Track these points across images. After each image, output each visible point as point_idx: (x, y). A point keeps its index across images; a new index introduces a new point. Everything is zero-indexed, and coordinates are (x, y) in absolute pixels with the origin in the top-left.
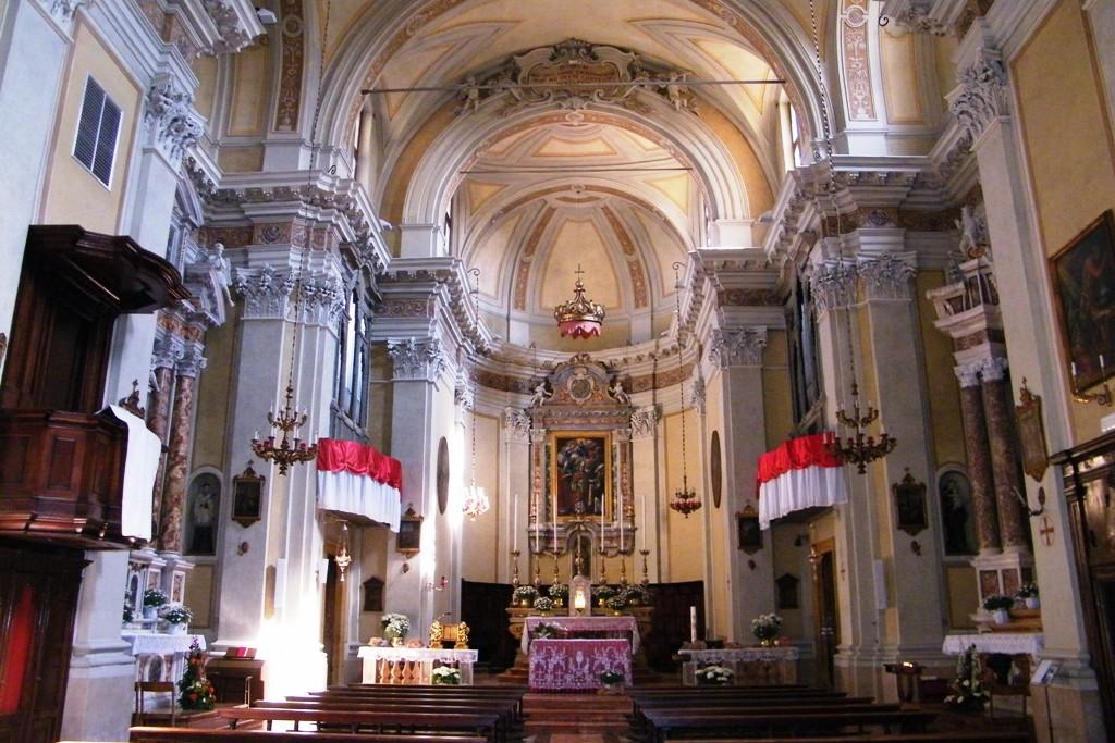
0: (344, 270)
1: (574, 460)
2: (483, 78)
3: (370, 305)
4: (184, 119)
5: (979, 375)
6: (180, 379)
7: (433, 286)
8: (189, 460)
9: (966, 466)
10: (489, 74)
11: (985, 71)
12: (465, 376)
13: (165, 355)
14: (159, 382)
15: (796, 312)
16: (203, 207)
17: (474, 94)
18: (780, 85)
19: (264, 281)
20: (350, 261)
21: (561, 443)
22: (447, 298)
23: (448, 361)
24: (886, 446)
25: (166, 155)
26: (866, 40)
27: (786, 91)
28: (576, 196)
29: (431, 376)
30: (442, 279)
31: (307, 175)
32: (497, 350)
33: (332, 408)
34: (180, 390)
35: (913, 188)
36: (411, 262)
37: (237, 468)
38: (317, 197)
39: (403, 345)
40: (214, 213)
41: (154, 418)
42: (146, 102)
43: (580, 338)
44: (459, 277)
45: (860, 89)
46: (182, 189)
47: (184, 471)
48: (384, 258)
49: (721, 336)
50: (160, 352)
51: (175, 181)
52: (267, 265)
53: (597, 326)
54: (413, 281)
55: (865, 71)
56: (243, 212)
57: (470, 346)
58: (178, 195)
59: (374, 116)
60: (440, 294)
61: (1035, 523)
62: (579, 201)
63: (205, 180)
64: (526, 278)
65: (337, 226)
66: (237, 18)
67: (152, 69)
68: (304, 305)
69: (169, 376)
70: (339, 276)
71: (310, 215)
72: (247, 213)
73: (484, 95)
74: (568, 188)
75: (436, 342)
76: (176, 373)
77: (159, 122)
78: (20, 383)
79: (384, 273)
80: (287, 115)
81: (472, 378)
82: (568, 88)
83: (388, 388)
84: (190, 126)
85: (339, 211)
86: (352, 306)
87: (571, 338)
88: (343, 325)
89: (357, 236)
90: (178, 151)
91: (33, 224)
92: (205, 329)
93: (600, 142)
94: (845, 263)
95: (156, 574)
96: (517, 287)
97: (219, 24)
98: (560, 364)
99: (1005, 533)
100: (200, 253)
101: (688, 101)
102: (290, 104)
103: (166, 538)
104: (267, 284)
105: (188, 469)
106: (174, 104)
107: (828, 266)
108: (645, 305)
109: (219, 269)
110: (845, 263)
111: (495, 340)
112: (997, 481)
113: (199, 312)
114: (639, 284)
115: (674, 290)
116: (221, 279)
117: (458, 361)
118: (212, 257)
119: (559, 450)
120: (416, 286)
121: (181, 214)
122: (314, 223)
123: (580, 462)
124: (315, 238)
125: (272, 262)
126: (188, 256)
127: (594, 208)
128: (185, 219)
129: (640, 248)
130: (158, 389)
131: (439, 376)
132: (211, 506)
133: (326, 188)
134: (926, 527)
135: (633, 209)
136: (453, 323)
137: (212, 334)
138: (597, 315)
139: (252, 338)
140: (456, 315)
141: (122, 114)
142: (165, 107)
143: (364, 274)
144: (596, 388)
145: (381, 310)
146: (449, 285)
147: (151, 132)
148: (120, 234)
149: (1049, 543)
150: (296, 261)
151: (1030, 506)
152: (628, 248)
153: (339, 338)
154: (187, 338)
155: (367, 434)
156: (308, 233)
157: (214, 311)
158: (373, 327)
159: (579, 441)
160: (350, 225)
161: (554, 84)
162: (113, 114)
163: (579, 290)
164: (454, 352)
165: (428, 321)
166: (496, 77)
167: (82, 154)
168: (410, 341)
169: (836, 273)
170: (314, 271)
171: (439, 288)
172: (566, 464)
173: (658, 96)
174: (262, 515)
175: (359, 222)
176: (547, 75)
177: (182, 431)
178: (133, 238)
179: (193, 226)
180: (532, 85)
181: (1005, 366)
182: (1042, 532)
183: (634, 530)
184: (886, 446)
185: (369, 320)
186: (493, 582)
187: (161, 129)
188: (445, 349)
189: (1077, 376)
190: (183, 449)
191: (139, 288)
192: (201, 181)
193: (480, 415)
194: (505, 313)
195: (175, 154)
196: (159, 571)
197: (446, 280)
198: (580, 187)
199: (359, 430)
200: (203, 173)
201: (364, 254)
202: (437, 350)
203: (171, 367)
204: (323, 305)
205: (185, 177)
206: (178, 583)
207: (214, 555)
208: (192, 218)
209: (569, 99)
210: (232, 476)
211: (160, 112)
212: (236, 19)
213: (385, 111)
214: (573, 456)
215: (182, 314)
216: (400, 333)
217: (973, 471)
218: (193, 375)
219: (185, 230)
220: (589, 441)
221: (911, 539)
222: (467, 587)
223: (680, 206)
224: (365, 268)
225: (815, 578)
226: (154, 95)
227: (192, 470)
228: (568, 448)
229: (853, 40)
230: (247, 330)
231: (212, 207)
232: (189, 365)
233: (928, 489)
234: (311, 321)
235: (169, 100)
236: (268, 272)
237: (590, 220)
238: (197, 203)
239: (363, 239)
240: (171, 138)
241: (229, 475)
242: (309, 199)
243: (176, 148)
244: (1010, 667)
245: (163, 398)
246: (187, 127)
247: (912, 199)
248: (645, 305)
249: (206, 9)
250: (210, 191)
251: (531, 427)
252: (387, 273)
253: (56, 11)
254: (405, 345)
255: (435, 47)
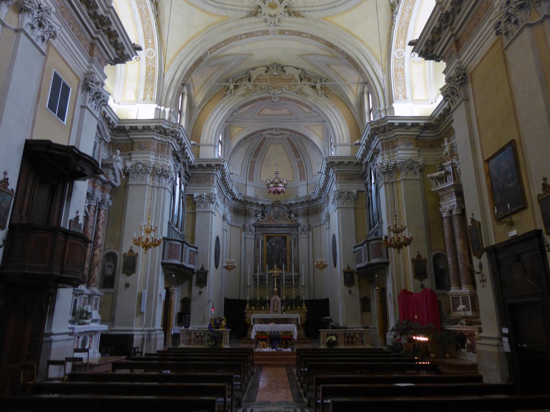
0: (174, 163)
1: (274, 246)
2: (236, 79)
3: (186, 179)
4: (100, 93)
5: (451, 211)
6: (99, 210)
7: (214, 170)
8: (103, 246)
9: (445, 251)
10: (238, 78)
11: (458, 77)
12: (227, 210)
13: (92, 199)
14: (89, 211)
15: (369, 183)
16: (110, 133)
17: (232, 87)
18: (365, 84)
19: (138, 167)
20: (178, 159)
21: (268, 238)
22: (220, 176)
23: (220, 203)
24: (408, 242)
25: (92, 110)
26: (403, 64)
27: (368, 87)
28: (276, 133)
29: (212, 209)
30: (218, 168)
31: (158, 121)
32: (241, 198)
33: (169, 223)
34: (99, 215)
35: (423, 130)
36: (205, 160)
37: (125, 249)
38: (162, 130)
39: (201, 196)
40: (115, 136)
41: (87, 227)
42: (82, 85)
43: (276, 194)
44: (225, 167)
45: (400, 86)
46: (100, 125)
47: (100, 251)
48: (192, 158)
49: (337, 193)
50: (90, 198)
51: (96, 122)
52: (140, 160)
53: (284, 189)
54: (205, 168)
55: (403, 78)
56: (129, 136)
57: (229, 197)
58: (98, 127)
59: (188, 95)
60: (217, 174)
61: (477, 277)
62: (277, 135)
63: (111, 121)
64: (254, 167)
65: (172, 144)
66: (118, 36)
67: (85, 70)
68: (156, 178)
69: (94, 209)
70: (172, 166)
71: (159, 139)
72: (131, 137)
73: (236, 87)
74: (272, 129)
75: (215, 195)
76: (97, 207)
77: (88, 94)
78: (21, 212)
79: (192, 165)
80: (149, 93)
81: (230, 210)
82: (273, 85)
83: (194, 214)
84: (103, 96)
85: (172, 137)
86: (178, 179)
87: (273, 194)
88: (174, 187)
89: (180, 148)
90: (98, 108)
91: (27, 138)
92: (111, 188)
93: (286, 109)
94: (392, 162)
95: (86, 298)
96: (250, 171)
97: (117, 49)
98: (268, 205)
99: (463, 280)
100: (109, 154)
101: (324, 92)
102: (150, 89)
103: (91, 281)
104: (139, 168)
105: (103, 250)
106: (96, 86)
107: (384, 164)
108: (304, 180)
109: (118, 161)
110: (392, 162)
111: (240, 194)
112: (459, 258)
113: (108, 180)
114: (302, 171)
115: (317, 173)
116: (119, 166)
117: (224, 203)
118: (114, 156)
119: (267, 241)
120: (206, 171)
121: (100, 136)
122: (161, 142)
123: (276, 247)
124: (161, 149)
125: (142, 159)
126: (102, 156)
127: (283, 138)
128: (102, 139)
129: (302, 155)
130: (89, 214)
131: (216, 210)
132: (113, 266)
133: (167, 127)
134: (427, 278)
135: (300, 139)
136: (222, 187)
137: (114, 191)
138: (284, 184)
139: (133, 193)
140: (224, 183)
141: (71, 90)
142: (92, 87)
143: (183, 165)
144: (283, 215)
145: (191, 181)
146: (221, 171)
147: (85, 98)
148: (70, 144)
149: (484, 286)
150: (153, 159)
151: (475, 270)
152: (298, 156)
153: (172, 193)
154: (103, 192)
155: (184, 235)
156: (158, 147)
157: (115, 180)
158: (187, 188)
159: (276, 238)
160: (177, 143)
161: (267, 83)
162: (66, 89)
163: (277, 173)
164: (223, 199)
165: (211, 186)
166: (241, 80)
167: (52, 106)
168: (203, 194)
169: (388, 167)
170: (161, 163)
171: (216, 172)
172: (270, 247)
173: (312, 89)
174: (137, 271)
175: (181, 142)
176: (263, 79)
177: (100, 234)
178: (77, 147)
179: (106, 142)
180: (257, 83)
181: (463, 207)
182: (481, 281)
183: (299, 276)
184: (408, 242)
185: (185, 185)
186: (238, 298)
187: (90, 97)
188: (218, 198)
189: (497, 213)
190: (100, 241)
191: (79, 169)
192: (109, 122)
193: (233, 226)
194: (245, 182)
195: (96, 108)
196: (87, 296)
197: (219, 168)
198: (277, 129)
199: (181, 233)
200: (110, 118)
201: (183, 156)
202: (215, 198)
203: (95, 204)
204: (165, 178)
205: (101, 119)
206: (96, 302)
207: (114, 288)
208: (105, 138)
209: (273, 90)
210: (123, 253)
211: (89, 89)
212: (124, 48)
213: (193, 93)
214: (273, 244)
215: (100, 181)
216: (199, 191)
217: (448, 253)
218: (106, 209)
219: (102, 144)
220: (280, 238)
221: (420, 283)
222: (227, 301)
223: (320, 137)
224: (184, 162)
225: (378, 299)
226: (86, 82)
227: (104, 250)
228: (271, 241)
229: (398, 64)
230: (130, 188)
231: (114, 133)
232: (103, 204)
233: (428, 261)
234: (159, 185)
235: (94, 84)
236: (140, 163)
237: (281, 143)
238: (107, 132)
239: (183, 150)
240: (94, 102)
241: (121, 252)
242: (159, 131)
243: (97, 107)
244: (466, 341)
245: (91, 219)
246: (102, 97)
247: (422, 135)
248: (304, 180)
249: (110, 43)
250: (113, 126)
251: (255, 232)
252: (193, 165)
253: (38, 40)
254: (201, 196)
255: (215, 65)
